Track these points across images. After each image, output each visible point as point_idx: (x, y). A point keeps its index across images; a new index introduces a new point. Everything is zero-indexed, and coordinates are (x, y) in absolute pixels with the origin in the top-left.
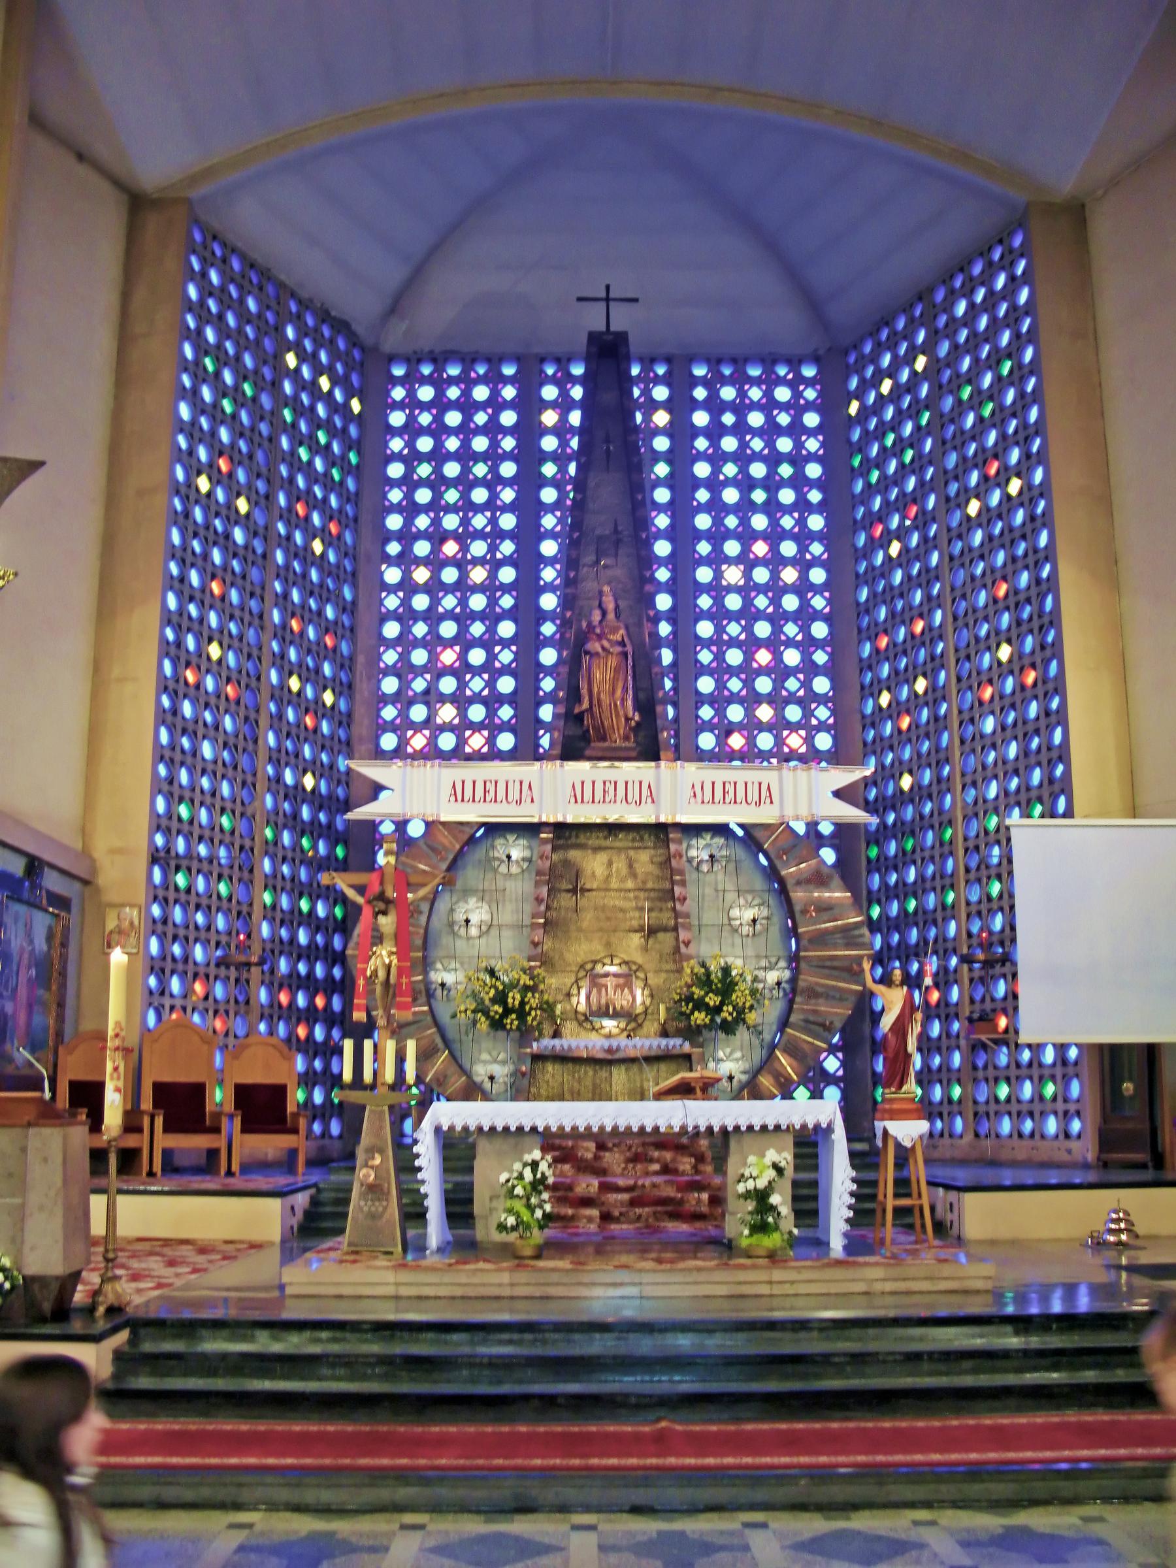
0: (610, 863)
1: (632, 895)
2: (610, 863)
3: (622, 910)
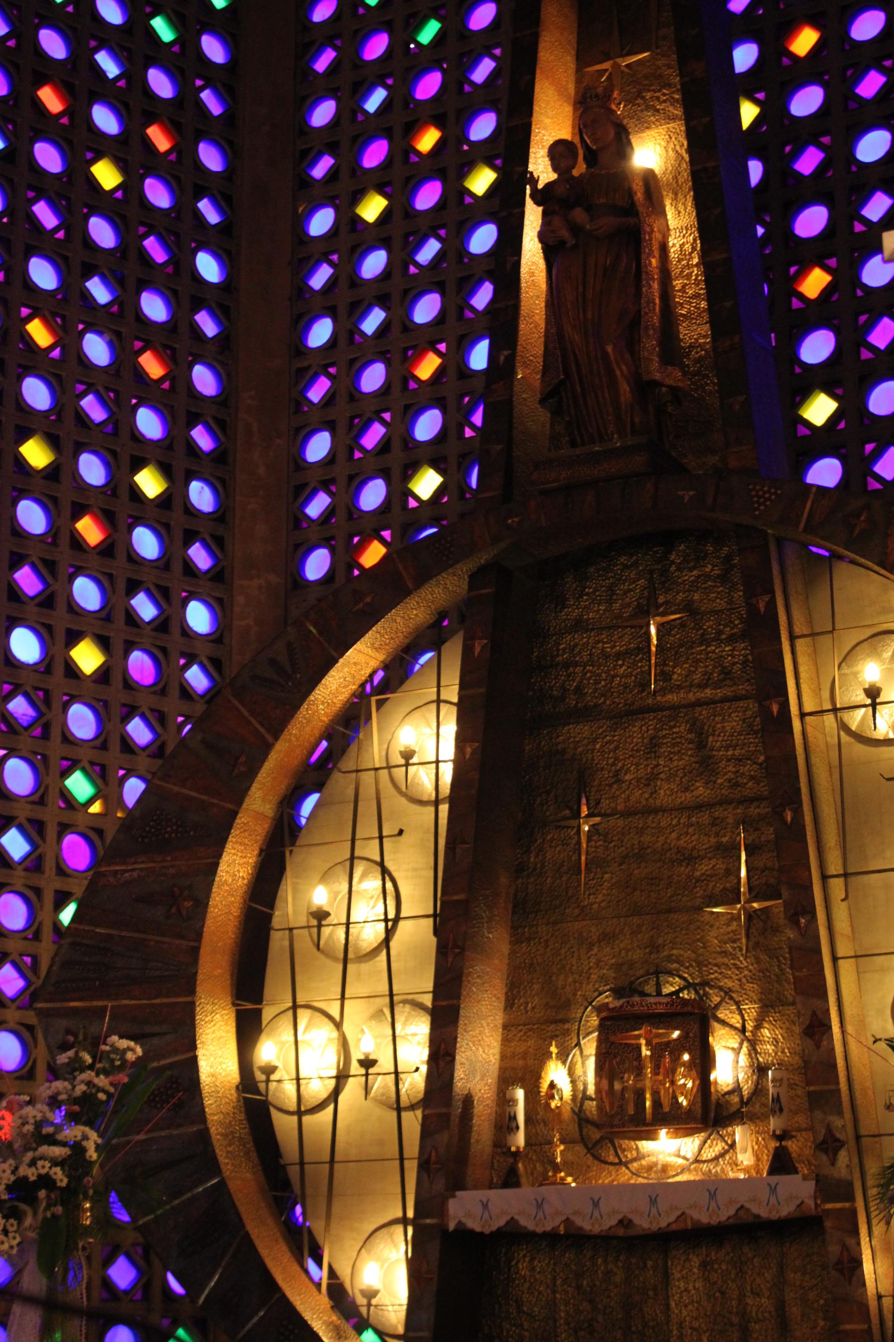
0: (653, 746)
1: (705, 818)
2: (653, 746)
3: (689, 858)
